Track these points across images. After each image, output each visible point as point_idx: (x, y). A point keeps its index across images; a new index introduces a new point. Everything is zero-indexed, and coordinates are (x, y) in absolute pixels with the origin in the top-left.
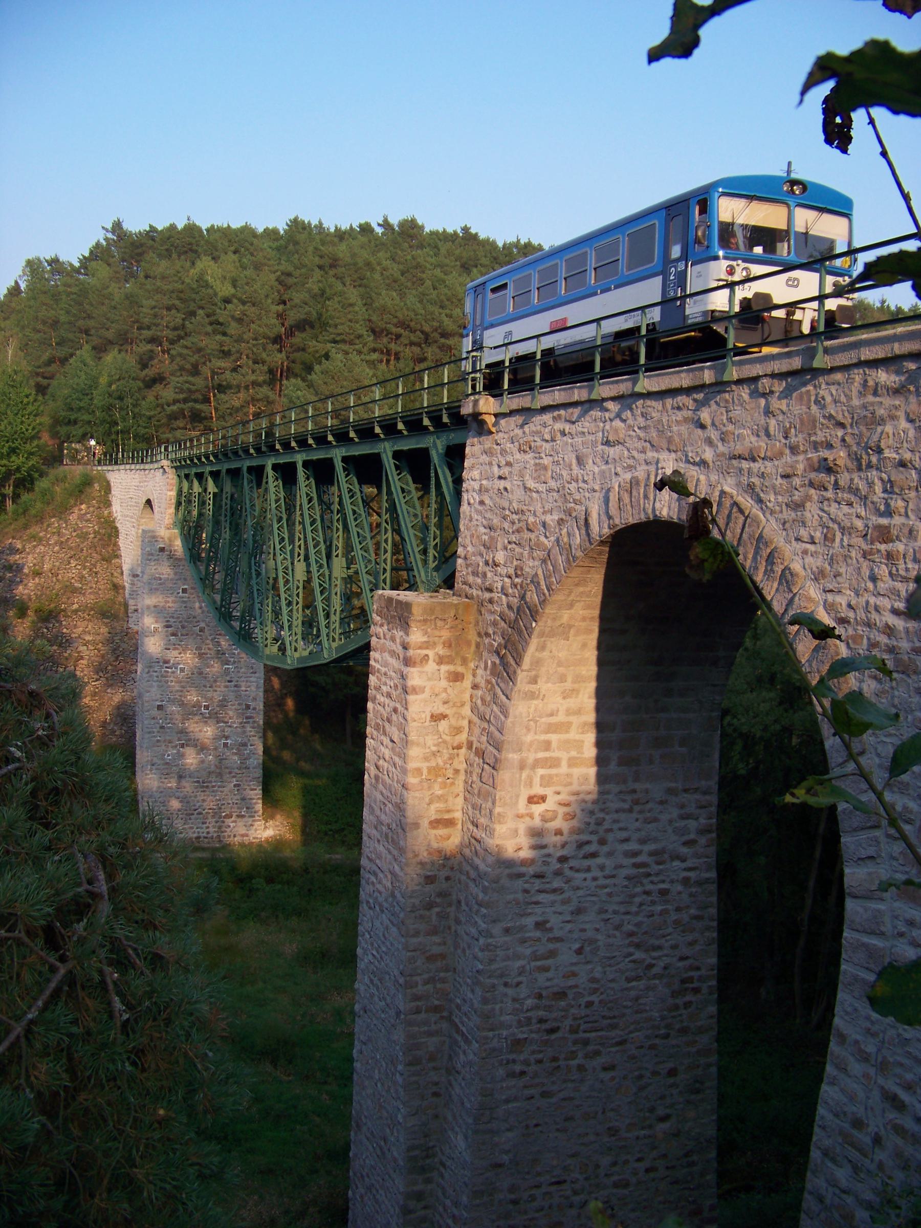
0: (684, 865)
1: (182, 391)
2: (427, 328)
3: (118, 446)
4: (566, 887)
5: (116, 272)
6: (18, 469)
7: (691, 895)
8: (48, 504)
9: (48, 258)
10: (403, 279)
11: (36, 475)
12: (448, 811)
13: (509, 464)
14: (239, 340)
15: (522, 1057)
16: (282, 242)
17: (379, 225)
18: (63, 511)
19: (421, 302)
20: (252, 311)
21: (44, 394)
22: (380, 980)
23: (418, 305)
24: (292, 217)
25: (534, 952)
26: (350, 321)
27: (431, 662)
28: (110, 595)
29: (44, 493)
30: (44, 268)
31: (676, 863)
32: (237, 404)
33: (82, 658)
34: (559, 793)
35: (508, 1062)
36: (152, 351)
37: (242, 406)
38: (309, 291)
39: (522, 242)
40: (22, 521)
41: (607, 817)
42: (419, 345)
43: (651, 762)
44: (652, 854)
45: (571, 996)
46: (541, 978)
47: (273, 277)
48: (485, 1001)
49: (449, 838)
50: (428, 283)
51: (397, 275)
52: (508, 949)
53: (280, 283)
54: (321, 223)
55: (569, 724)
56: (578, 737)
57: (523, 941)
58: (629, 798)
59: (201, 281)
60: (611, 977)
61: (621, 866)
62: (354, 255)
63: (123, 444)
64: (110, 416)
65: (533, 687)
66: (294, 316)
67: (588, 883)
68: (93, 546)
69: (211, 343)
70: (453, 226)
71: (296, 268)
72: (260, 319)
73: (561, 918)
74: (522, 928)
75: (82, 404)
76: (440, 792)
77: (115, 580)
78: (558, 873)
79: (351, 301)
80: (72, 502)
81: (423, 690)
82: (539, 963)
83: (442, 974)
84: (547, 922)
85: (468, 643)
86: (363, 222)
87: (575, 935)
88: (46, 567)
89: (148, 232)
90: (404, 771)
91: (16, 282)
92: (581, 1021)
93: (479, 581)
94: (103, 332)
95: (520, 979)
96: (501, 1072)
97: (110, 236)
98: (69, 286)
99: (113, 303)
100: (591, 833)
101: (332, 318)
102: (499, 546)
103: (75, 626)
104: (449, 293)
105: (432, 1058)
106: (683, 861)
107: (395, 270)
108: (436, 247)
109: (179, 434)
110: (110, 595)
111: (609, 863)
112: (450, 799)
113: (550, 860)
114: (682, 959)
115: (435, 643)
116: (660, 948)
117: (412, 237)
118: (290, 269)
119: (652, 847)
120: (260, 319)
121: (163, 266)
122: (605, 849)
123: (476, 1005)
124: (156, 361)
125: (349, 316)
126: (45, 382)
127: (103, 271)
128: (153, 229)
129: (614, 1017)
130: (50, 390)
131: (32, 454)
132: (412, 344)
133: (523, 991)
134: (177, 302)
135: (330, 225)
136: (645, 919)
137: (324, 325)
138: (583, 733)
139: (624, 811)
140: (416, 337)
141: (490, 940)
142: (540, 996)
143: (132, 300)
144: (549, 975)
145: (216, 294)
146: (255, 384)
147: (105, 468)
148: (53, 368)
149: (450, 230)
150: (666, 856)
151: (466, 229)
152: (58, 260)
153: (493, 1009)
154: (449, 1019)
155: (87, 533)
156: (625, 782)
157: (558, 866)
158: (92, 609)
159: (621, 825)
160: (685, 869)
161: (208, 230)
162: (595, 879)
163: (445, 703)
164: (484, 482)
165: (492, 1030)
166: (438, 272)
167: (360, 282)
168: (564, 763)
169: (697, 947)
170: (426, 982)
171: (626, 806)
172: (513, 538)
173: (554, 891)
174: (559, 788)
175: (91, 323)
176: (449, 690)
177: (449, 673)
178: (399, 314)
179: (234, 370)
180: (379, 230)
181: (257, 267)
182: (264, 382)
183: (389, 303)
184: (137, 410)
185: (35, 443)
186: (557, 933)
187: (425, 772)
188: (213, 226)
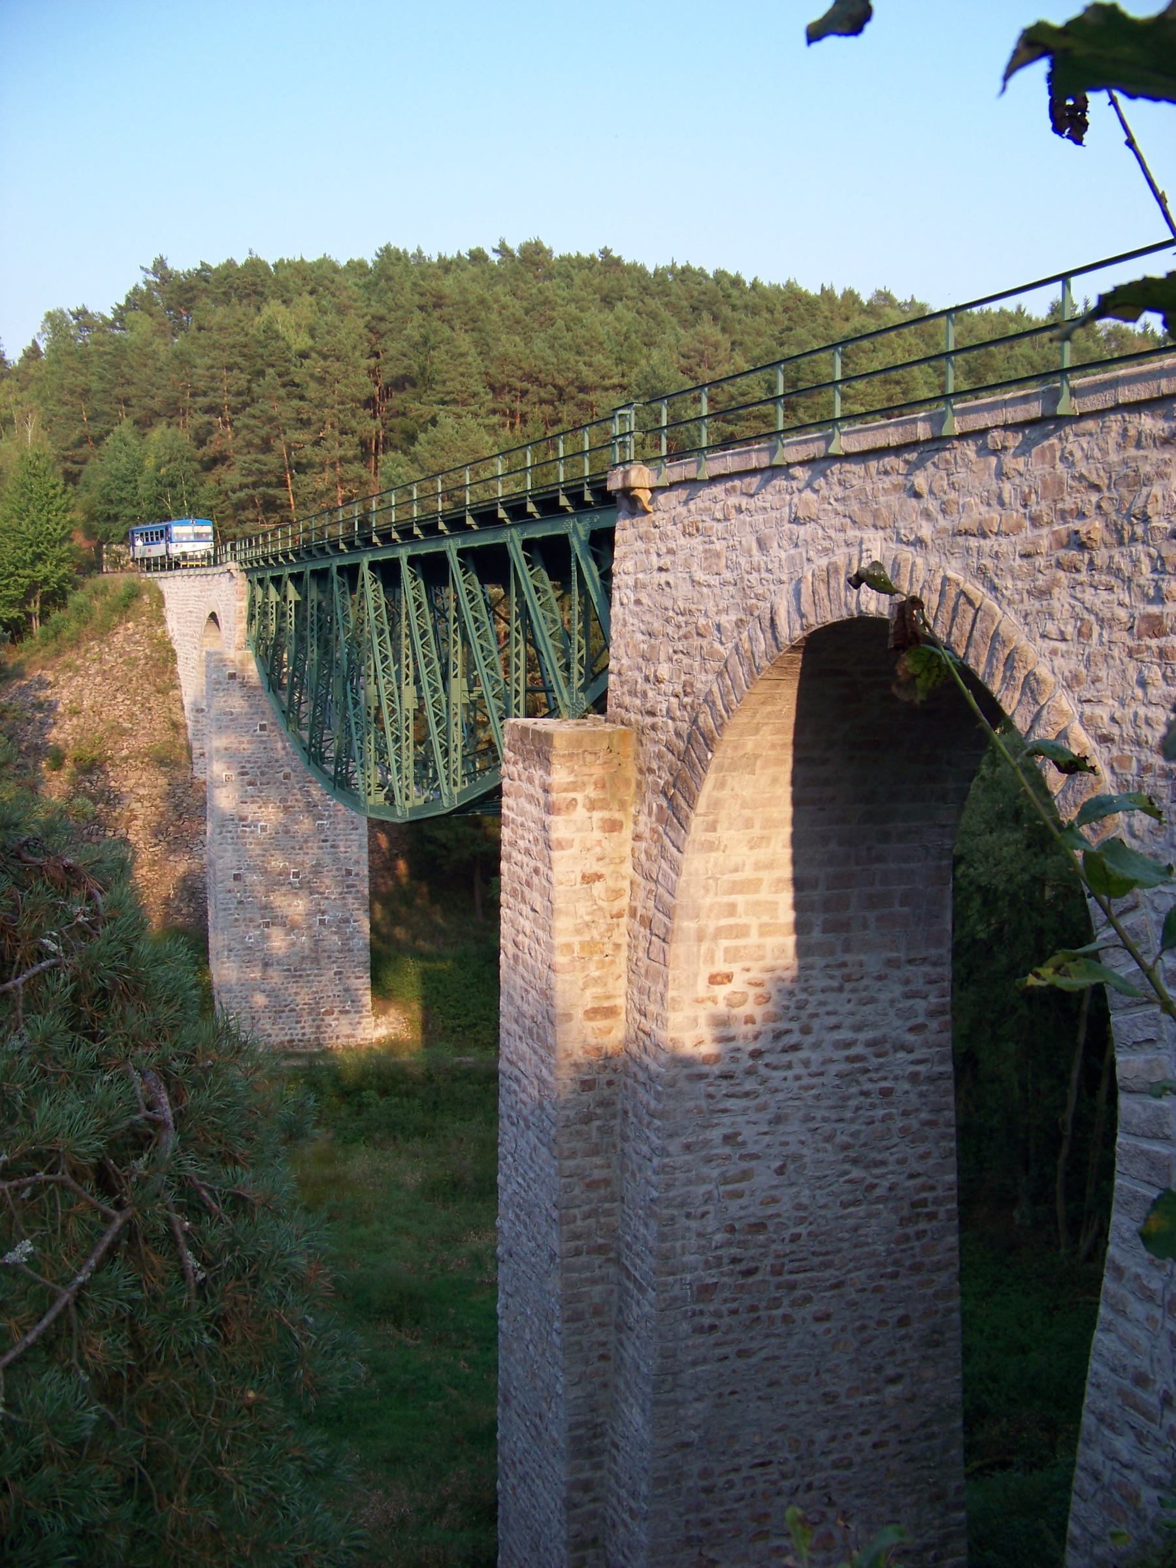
0: (911, 1057)
1: (250, 473)
2: (561, 382)
4: (761, 1089)
6: (46, 581)
7: (921, 1095)
9: (73, 309)
10: (527, 319)
11: (69, 587)
12: (608, 997)
13: (671, 552)
14: (321, 405)
17: (495, 251)
18: (105, 631)
19: (552, 347)
20: (335, 367)
22: (529, 1215)
23: (549, 351)
24: (383, 245)
25: (723, 1174)
26: (462, 375)
27: (580, 807)
28: (169, 736)
29: (79, 610)
31: (901, 1055)
32: (321, 486)
33: (136, 818)
36: (210, 423)
38: (408, 338)
39: (679, 266)
40: (53, 646)
41: (811, 999)
42: (551, 403)
44: (868, 1044)
45: (771, 1228)
46: (733, 1206)
47: (361, 323)
48: (663, 1237)
49: (609, 1032)
50: (560, 323)
51: (520, 313)
52: (689, 1171)
54: (420, 252)
56: (770, 897)
57: (709, 1160)
59: (271, 333)
60: (822, 1202)
61: (831, 1061)
62: (463, 291)
65: (711, 836)
66: (390, 372)
68: (145, 675)
69: (285, 410)
70: (589, 249)
71: (390, 310)
72: (347, 377)
73: (756, 1128)
74: (706, 1143)
75: (123, 495)
76: (597, 974)
77: (174, 717)
78: (750, 1072)
79: (462, 350)
80: (116, 619)
82: (729, 1187)
83: (607, 1205)
85: (627, 782)
86: (473, 248)
88: (86, 704)
89: (199, 272)
90: (550, 948)
91: (34, 342)
92: (786, 1260)
93: (638, 702)
96: (685, 1327)
97: (151, 278)
98: (102, 344)
99: (159, 364)
100: (791, 1019)
101: (438, 372)
102: (662, 657)
103: (126, 778)
104: (588, 335)
105: (597, 1312)
106: (911, 1051)
107: (516, 307)
108: (569, 276)
109: (248, 528)
110: (169, 736)
111: (815, 1057)
112: (610, 981)
114: (911, 1176)
116: (883, 1163)
117: (537, 265)
118: (383, 311)
119: (869, 1035)
121: (219, 315)
122: (810, 1039)
123: (651, 1243)
124: (216, 436)
125: (461, 370)
126: (75, 468)
127: (144, 323)
128: (205, 267)
129: (827, 1253)
130: (83, 478)
131: (62, 560)
132: (542, 402)
133: (711, 1224)
134: (239, 360)
135: (432, 254)
137: (429, 382)
139: (832, 989)
140: (547, 393)
141: (666, 1160)
142: (732, 1229)
143: (182, 360)
144: (743, 1201)
145: (289, 348)
146: (343, 460)
147: (156, 575)
148: (86, 449)
149: (586, 254)
151: (605, 253)
152: (86, 312)
153: (673, 1248)
154: (617, 1261)
155: (137, 659)
157: (751, 1062)
158: (146, 755)
159: (829, 1008)
161: (275, 266)
162: (798, 1078)
163: (599, 859)
164: (640, 576)
167: (474, 325)
168: (754, 931)
172: (680, 646)
173: (747, 1095)
174: (748, 964)
175: (131, 390)
176: (605, 843)
178: (523, 365)
179: (316, 443)
180: (495, 258)
181: (341, 311)
182: (355, 457)
183: (511, 350)
184: (193, 500)
185: (66, 546)
186: (752, 1149)
187: (577, 948)
188: (282, 261)
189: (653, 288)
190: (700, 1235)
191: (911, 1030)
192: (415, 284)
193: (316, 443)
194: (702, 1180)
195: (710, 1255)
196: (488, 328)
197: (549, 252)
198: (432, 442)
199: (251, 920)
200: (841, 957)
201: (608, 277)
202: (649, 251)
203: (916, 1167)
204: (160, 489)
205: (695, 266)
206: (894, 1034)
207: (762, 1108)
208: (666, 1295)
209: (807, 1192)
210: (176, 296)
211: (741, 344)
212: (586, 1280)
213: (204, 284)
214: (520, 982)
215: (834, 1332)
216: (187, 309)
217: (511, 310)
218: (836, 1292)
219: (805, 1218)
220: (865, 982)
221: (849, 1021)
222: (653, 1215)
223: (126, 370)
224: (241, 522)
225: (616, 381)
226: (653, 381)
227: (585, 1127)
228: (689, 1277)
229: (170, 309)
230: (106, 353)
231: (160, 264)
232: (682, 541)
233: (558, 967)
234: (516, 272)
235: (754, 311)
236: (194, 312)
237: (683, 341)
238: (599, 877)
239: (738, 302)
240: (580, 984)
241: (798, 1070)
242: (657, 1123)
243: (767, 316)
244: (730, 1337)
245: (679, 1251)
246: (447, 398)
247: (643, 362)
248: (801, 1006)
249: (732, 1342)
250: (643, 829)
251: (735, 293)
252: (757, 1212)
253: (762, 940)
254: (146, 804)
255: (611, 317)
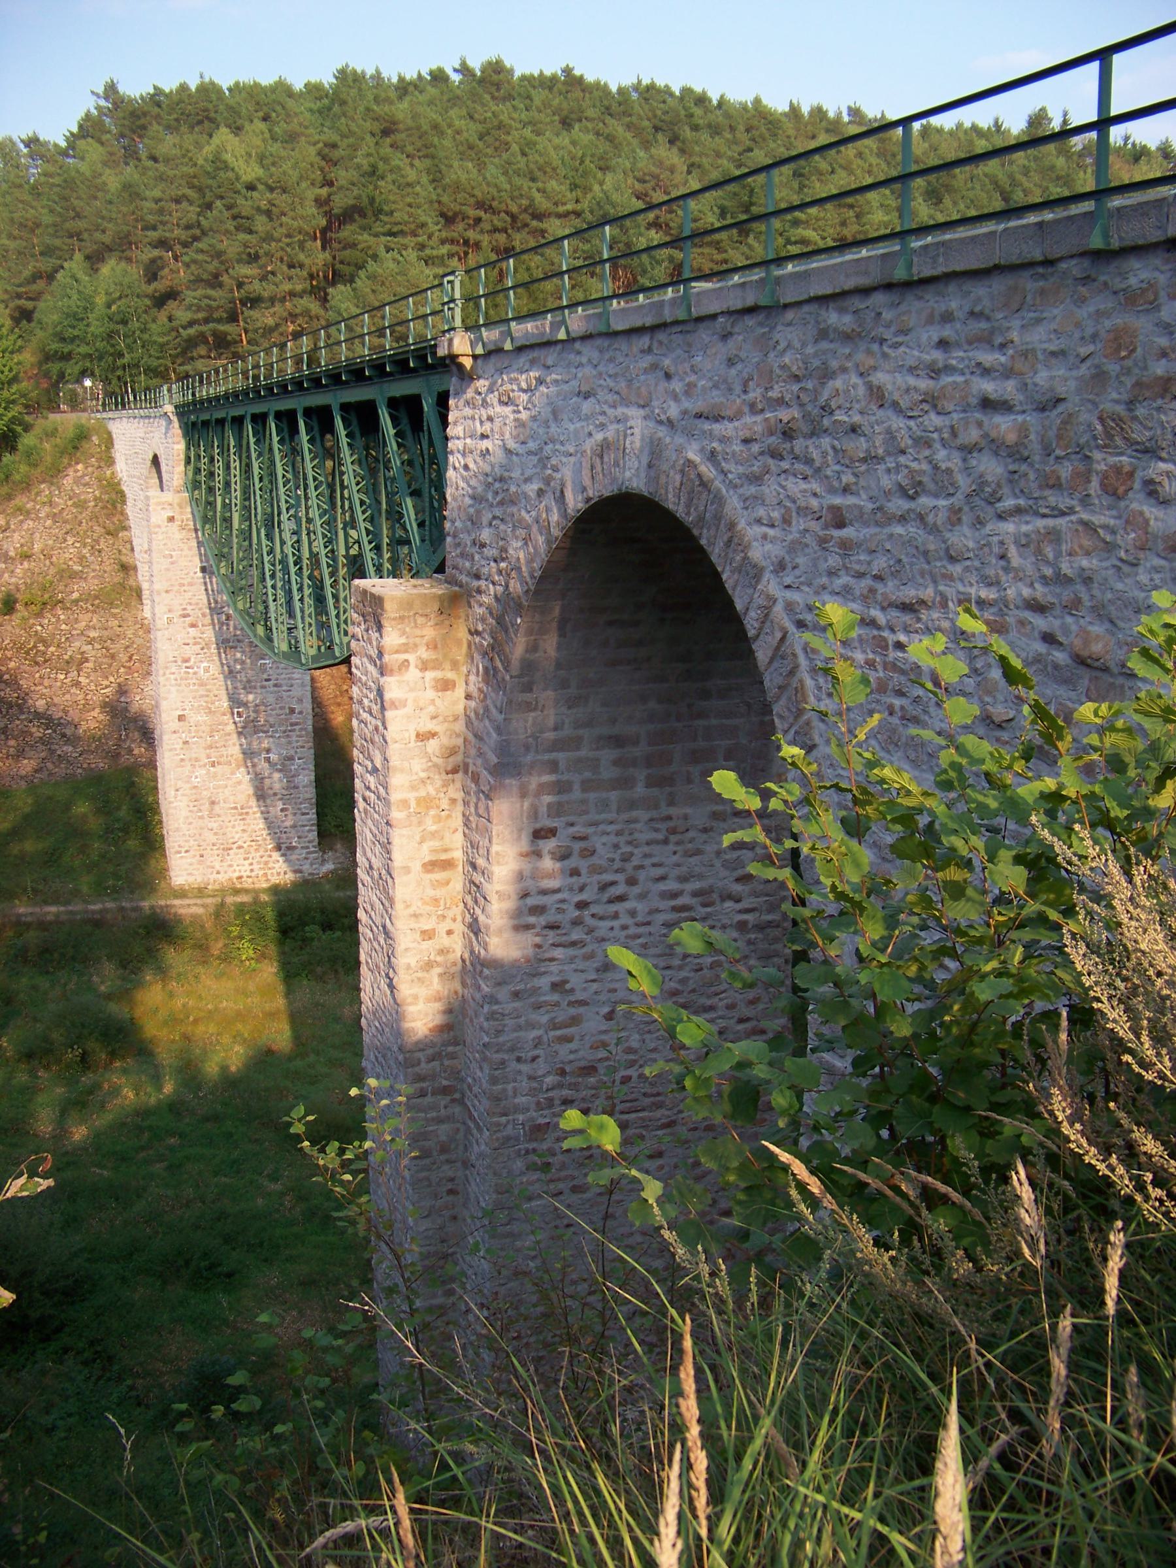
1: (199, 309)
2: (514, 209)
3: (126, 384)
4: (588, 938)
5: (111, 154)
7: (749, 942)
8: (36, 466)
9: (24, 137)
10: (481, 144)
11: (19, 429)
12: (446, 850)
13: (490, 419)
14: (268, 238)
15: (545, 1146)
16: (326, 101)
17: (455, 70)
18: (55, 473)
19: (505, 173)
20: (282, 200)
21: (30, 320)
22: (384, 1056)
23: (502, 178)
24: (339, 67)
25: (553, 1019)
26: (410, 205)
27: (412, 668)
28: (118, 578)
29: (29, 454)
30: (18, 152)
31: (729, 904)
32: (270, 321)
33: (87, 660)
34: (572, 825)
35: (527, 1152)
36: (161, 258)
37: (277, 325)
38: (359, 167)
39: (644, 83)
41: (636, 851)
42: (505, 231)
43: (689, 781)
44: (695, 894)
45: (602, 1071)
46: (564, 1051)
47: (312, 151)
48: (494, 1081)
49: (448, 883)
50: (515, 148)
51: (474, 139)
52: (519, 1017)
53: (323, 158)
54: (378, 72)
55: (580, 739)
56: (591, 754)
57: (538, 1007)
58: (663, 826)
59: (219, 163)
60: (653, 1045)
61: (658, 911)
62: (415, 116)
63: (133, 381)
64: (113, 346)
65: (527, 697)
66: (340, 202)
67: (616, 932)
68: (94, 517)
69: (231, 246)
70: (552, 68)
71: (343, 136)
72: (293, 210)
73: (584, 976)
74: (535, 991)
75: (76, 332)
76: (434, 828)
77: (123, 558)
78: (576, 922)
79: (409, 179)
80: (66, 461)
81: (404, 703)
82: (559, 1033)
83: (450, 1049)
84: (566, 982)
86: (434, 67)
87: (603, 997)
88: (37, 547)
89: (153, 96)
90: (387, 803)
94: (98, 235)
95: (536, 1052)
96: (519, 1164)
97: (103, 103)
98: (51, 175)
99: (108, 197)
100: (617, 871)
101: (386, 201)
102: (485, 521)
103: (77, 621)
104: (541, 160)
105: (444, 1150)
106: (738, 901)
107: (471, 131)
108: (529, 97)
109: (200, 365)
110: (118, 578)
112: (447, 835)
113: (564, 906)
114: (741, 1021)
115: (416, 645)
116: (712, 1008)
117: (498, 86)
118: (335, 138)
119: (696, 885)
120: (293, 210)
121: (168, 144)
122: (636, 890)
123: (485, 1085)
124: (166, 270)
125: (409, 200)
126: (29, 305)
127: (94, 151)
128: (158, 91)
129: (658, 1094)
130: (36, 315)
131: (13, 402)
132: (496, 230)
133: (541, 1067)
134: (189, 192)
135: (391, 74)
136: (692, 974)
138: (597, 749)
139: (657, 842)
141: (495, 1007)
142: (563, 1073)
143: (130, 192)
144: (572, 1046)
145: (238, 179)
146: (292, 294)
147: (105, 415)
148: (41, 284)
149: (548, 73)
150: (715, 896)
151: (568, 71)
152: (38, 140)
153: (504, 1090)
154: (461, 1102)
155: (85, 502)
156: (656, 807)
157: (577, 913)
158: (96, 597)
159: (655, 860)
160: (740, 912)
161: (230, 90)
163: (433, 718)
164: (468, 441)
165: (505, 1115)
166: (528, 132)
167: (427, 152)
169: (761, 1006)
170: (431, 1059)
171: (660, 836)
172: (498, 512)
173: (573, 944)
174: (571, 819)
175: (81, 224)
176: (438, 702)
177: (437, 681)
178: (477, 192)
179: (263, 278)
180: (456, 78)
181: (291, 138)
182: (304, 291)
183: (464, 177)
184: (146, 336)
185: (15, 388)
186: (580, 996)
187: (413, 804)
188: (237, 84)
189: (615, 108)
190: (531, 1078)
191: (737, 880)
192: (368, 109)
193: (263, 278)
194: (532, 1026)
195: (542, 1097)
196: (442, 154)
197: (511, 72)
198: (372, 277)
199: (197, 760)
200: (665, 811)
201: (569, 97)
202: (613, 68)
203: (747, 1012)
204: (112, 326)
205: (660, 83)
206: (720, 884)
207: (590, 956)
208: (499, 1135)
209: (637, 1036)
210: (127, 124)
211: (699, 166)
212: (433, 1119)
213: (157, 110)
214: (369, 836)
215: (666, 1169)
216: (140, 137)
217: (465, 134)
218: (668, 1130)
219: (635, 1061)
220: (691, 834)
221: (676, 872)
222: (485, 1059)
223: (76, 202)
224: (192, 359)
225: (569, 207)
226: (607, 207)
227: (425, 974)
228: (521, 1117)
229: (123, 136)
230: (53, 185)
231: (111, 89)
232: (498, 409)
233: (393, 822)
234: (474, 96)
235: (715, 130)
236: (146, 140)
237: (640, 165)
238: (433, 735)
239: (701, 122)
240: (418, 838)
241: (625, 920)
242: (486, 972)
243: (729, 136)
244: (563, 1174)
245: (510, 1093)
246: (395, 229)
247: (596, 188)
248: (626, 858)
249: (566, 1177)
250: (473, 689)
251: (698, 112)
252: (586, 1055)
253: (586, 795)
254: (97, 646)
255: (567, 141)
